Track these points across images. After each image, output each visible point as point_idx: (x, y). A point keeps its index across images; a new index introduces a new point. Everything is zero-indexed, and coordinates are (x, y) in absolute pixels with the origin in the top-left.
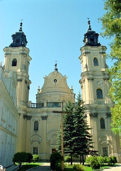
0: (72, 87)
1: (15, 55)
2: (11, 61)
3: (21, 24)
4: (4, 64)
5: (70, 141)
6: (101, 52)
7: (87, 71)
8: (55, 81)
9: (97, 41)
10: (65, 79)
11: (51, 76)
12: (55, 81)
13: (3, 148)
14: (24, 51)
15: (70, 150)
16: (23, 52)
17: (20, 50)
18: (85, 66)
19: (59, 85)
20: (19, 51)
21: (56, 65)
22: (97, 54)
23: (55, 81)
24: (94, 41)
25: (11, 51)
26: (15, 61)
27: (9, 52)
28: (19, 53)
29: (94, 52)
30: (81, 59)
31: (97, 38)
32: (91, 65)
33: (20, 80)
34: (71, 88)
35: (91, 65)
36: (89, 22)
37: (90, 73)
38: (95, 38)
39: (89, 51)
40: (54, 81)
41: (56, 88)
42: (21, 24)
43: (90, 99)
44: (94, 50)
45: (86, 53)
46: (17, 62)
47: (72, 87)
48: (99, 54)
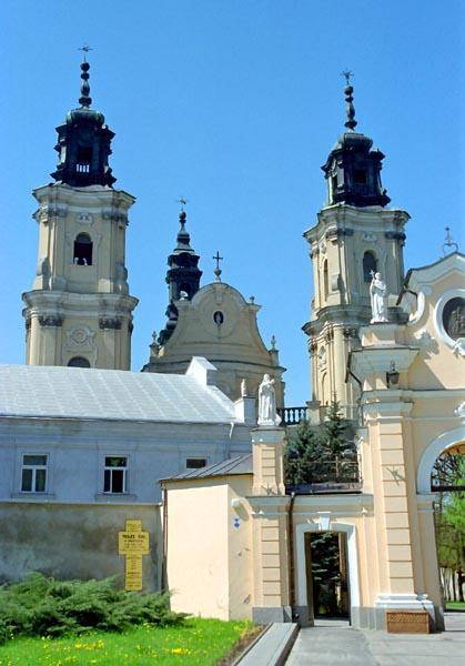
0: (273, 343)
1: (84, 221)
2: (69, 244)
3: (85, 67)
4: (46, 256)
5: (319, 544)
6: (390, 233)
7: (343, 304)
8: (218, 318)
9: (376, 183)
10: (251, 311)
11: (201, 302)
12: (218, 318)
13: (293, 602)
14: (117, 206)
15: (318, 568)
16: (115, 210)
17: (102, 200)
18: (335, 281)
19: (231, 334)
20: (98, 206)
21: (183, 218)
22: (375, 238)
23: (219, 317)
24: (365, 182)
25: (67, 203)
26: (85, 241)
27: (63, 206)
28: (97, 211)
29: (364, 229)
30: (311, 241)
31: (378, 167)
32: (357, 280)
33: (113, 323)
34: (269, 347)
35: (357, 280)
36: (350, 91)
37: (354, 311)
38: (371, 170)
39: (349, 226)
40: (215, 318)
41: (222, 346)
42: (85, 67)
43: (349, 402)
44: (368, 220)
45: (339, 232)
46: (91, 245)
47: (273, 343)
48: (383, 240)
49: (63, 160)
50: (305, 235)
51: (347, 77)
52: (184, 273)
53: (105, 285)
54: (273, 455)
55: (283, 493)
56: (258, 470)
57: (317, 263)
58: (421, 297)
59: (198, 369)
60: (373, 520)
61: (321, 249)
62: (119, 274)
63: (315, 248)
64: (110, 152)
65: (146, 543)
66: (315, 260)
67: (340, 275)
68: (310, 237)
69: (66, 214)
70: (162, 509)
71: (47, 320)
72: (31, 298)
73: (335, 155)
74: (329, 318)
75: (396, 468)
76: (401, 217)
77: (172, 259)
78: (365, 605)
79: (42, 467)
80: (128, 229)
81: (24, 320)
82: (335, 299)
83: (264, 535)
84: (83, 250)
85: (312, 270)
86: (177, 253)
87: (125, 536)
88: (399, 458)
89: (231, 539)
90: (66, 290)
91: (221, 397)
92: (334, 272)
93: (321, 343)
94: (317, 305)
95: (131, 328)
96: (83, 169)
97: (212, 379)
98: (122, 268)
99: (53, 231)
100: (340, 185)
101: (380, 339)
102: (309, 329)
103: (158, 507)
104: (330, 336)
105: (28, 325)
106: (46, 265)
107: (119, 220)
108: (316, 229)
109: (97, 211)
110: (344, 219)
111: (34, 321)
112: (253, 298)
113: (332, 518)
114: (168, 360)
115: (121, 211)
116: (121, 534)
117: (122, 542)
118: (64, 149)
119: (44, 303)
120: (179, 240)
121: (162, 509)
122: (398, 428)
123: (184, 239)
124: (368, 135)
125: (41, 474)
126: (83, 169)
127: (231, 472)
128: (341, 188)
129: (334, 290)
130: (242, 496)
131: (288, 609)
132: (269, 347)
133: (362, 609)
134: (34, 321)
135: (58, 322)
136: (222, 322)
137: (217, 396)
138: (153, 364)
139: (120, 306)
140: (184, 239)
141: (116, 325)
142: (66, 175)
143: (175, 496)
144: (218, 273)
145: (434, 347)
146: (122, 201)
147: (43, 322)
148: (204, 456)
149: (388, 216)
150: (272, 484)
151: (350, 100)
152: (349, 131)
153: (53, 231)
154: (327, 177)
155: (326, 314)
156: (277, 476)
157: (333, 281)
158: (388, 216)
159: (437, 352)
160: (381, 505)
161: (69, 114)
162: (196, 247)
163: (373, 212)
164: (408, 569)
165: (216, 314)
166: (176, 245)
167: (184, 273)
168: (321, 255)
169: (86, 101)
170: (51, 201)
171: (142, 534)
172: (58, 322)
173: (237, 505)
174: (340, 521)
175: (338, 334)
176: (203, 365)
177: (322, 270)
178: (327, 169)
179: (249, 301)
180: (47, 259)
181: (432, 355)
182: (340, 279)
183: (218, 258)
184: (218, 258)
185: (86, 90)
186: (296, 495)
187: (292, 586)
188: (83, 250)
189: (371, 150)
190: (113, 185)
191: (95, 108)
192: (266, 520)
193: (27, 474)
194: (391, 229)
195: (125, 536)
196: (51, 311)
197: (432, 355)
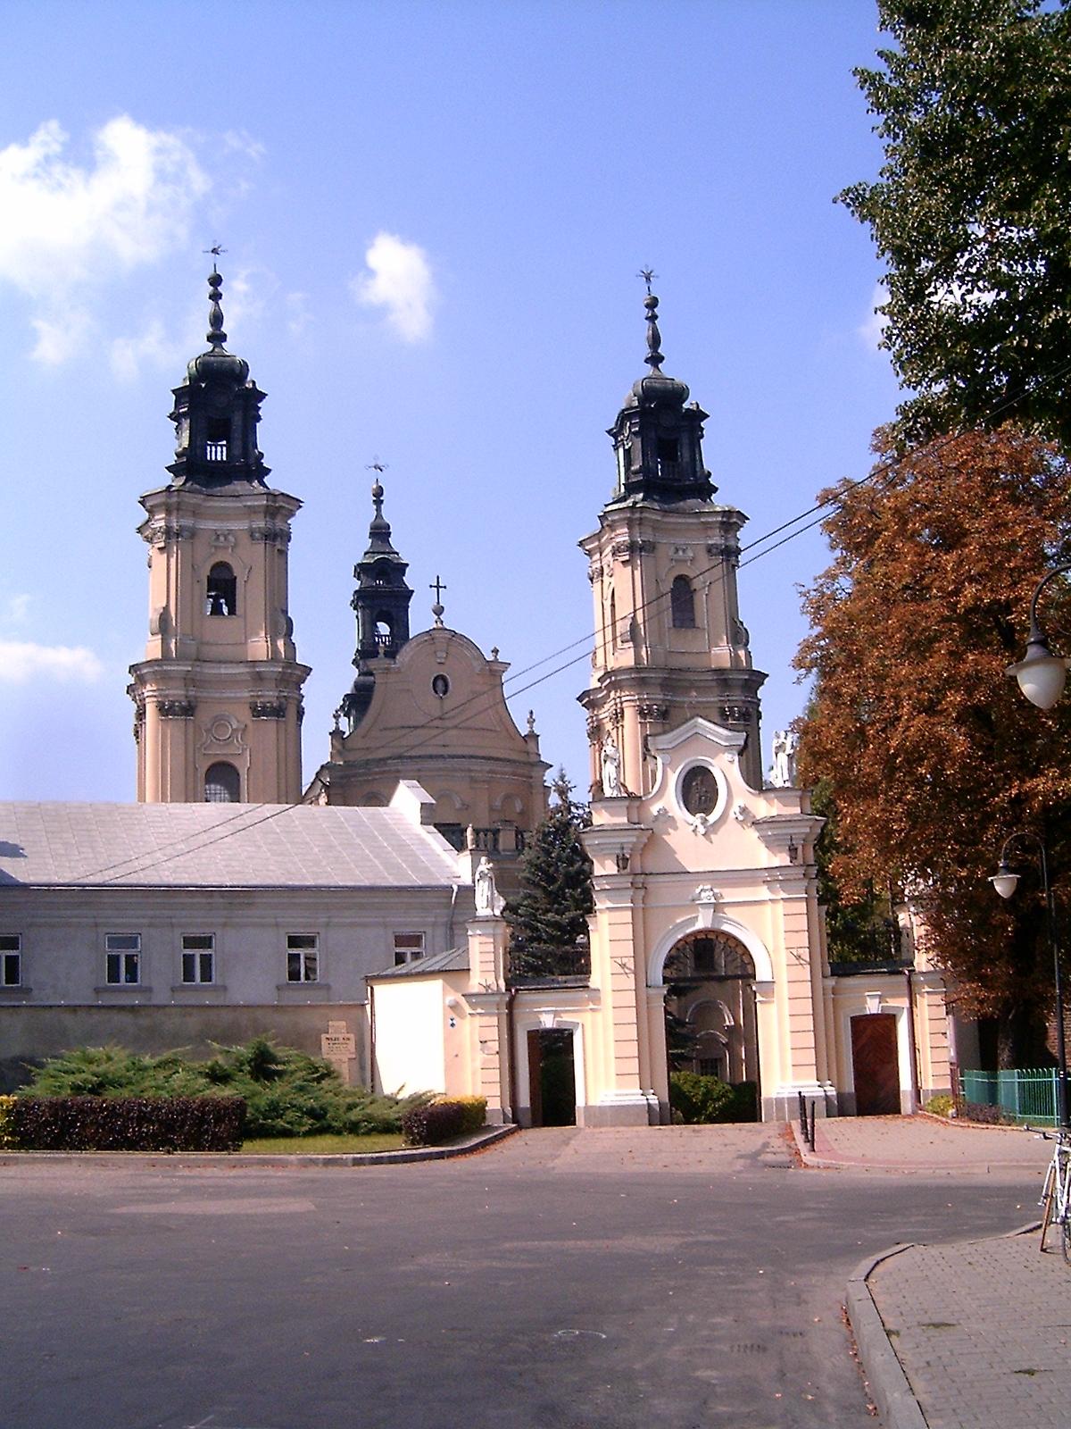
0: (531, 721)
3: (216, 281)
7: (637, 668)
8: (440, 683)
9: (694, 460)
10: (493, 671)
12: (440, 683)
30: (590, 553)
31: (696, 434)
34: (524, 731)
38: (685, 440)
45: (632, 548)
47: (531, 721)
49: (186, 444)
50: (581, 544)
51: (648, 279)
52: (382, 589)
53: (259, 647)
54: (491, 947)
55: (504, 990)
56: (475, 966)
58: (659, 761)
59: (408, 799)
60: (599, 1016)
62: (281, 625)
64: (258, 419)
65: (352, 1045)
66: (597, 585)
67: (634, 618)
69: (193, 534)
70: (368, 1007)
73: (624, 417)
74: (615, 686)
75: (625, 960)
76: (732, 520)
77: (361, 570)
78: (590, 1104)
80: (293, 548)
81: (133, 707)
82: (626, 658)
83: (481, 1030)
84: (222, 586)
85: (591, 602)
88: (628, 949)
89: (447, 1040)
90: (198, 660)
91: (442, 845)
92: (624, 609)
94: (600, 661)
95: (300, 713)
96: (217, 453)
97: (429, 815)
98: (283, 621)
99: (173, 561)
101: (612, 815)
102: (589, 700)
103: (364, 1005)
104: (618, 716)
105: (141, 715)
106: (164, 617)
107: (277, 539)
108: (598, 536)
109: (241, 525)
111: (151, 709)
112: (496, 651)
113: (556, 1013)
114: (356, 780)
115: (279, 524)
116: (324, 1036)
117: (324, 1043)
118: (186, 424)
119: (163, 678)
120: (372, 535)
121: (368, 1007)
122: (627, 916)
123: (380, 532)
124: (680, 379)
125: (206, 960)
126: (217, 453)
128: (636, 473)
130: (456, 991)
131: (509, 1110)
132: (524, 731)
133: (587, 1108)
134: (151, 709)
135: (188, 710)
136: (445, 692)
137: (436, 842)
140: (380, 532)
141: (278, 712)
142: (190, 466)
143: (382, 991)
144: (439, 611)
145: (671, 821)
146: (283, 507)
147: (163, 710)
148: (414, 931)
150: (491, 980)
151: (653, 318)
153: (173, 561)
155: (613, 680)
156: (496, 971)
157: (623, 627)
159: (676, 828)
160: (608, 999)
163: (683, 513)
164: (634, 1066)
165: (436, 679)
167: (382, 589)
168: (606, 578)
169: (217, 338)
170: (169, 512)
171: (348, 1036)
172: (188, 710)
173: (453, 1003)
174: (567, 1018)
175: (629, 713)
176: (418, 796)
177: (608, 604)
179: (490, 657)
180: (166, 609)
181: (670, 830)
182: (634, 625)
183: (438, 587)
184: (438, 587)
186: (517, 990)
188: (222, 586)
189: (685, 406)
192: (487, 1018)
193: (188, 960)
194: (716, 539)
196: (177, 693)
197: (670, 830)
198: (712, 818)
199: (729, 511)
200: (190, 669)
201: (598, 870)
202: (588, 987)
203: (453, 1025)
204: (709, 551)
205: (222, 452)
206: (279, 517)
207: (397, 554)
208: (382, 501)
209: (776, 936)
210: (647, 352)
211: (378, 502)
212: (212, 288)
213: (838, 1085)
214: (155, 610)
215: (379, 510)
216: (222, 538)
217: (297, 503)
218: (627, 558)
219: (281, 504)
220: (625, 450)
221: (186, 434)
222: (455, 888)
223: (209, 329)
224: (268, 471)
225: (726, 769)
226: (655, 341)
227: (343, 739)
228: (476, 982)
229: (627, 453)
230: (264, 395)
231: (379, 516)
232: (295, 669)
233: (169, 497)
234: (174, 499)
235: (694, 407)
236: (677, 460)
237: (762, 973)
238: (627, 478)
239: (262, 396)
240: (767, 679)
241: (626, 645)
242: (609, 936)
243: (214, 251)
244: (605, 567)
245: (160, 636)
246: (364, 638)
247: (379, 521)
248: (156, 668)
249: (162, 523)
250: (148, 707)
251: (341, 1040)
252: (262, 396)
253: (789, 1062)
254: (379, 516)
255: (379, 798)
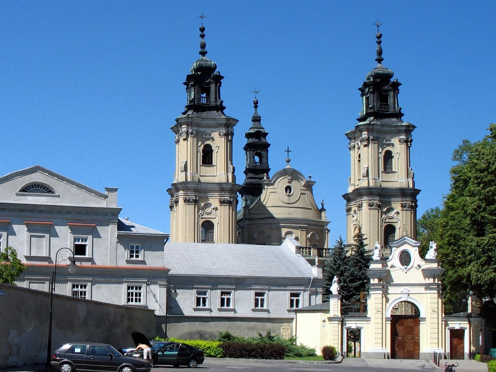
0: (322, 204)
57: (354, 154)
61: (356, 147)
63: (352, 144)
65: (289, 331)
68: (351, 136)
71: (189, 200)
72: (179, 186)
73: (366, 85)
79: (228, 297)
86: (252, 131)
87: (283, 328)
93: (354, 208)
100: (370, 106)
102: (348, 198)
104: (360, 206)
110: (372, 130)
116: (281, 328)
120: (253, 121)
123: (256, 119)
127: (322, 309)
128: (371, 108)
129: (364, 177)
137: (302, 261)
138: (246, 219)
139: (231, 190)
140: (256, 119)
149: (401, 128)
151: (379, 43)
152: (379, 65)
154: (362, 95)
158: (401, 128)
160: (373, 320)
161: (195, 64)
162: (266, 126)
166: (251, 124)
170: (188, 125)
173: (324, 320)
178: (362, 90)
180: (186, 162)
185: (203, 46)
187: (303, 367)
190: (224, 111)
191: (210, 59)
195: (283, 328)
198: (409, 267)
199: (409, 125)
200: (196, 186)
201: (372, 281)
202: (366, 317)
203: (324, 326)
204: (400, 141)
205: (204, 100)
206: (230, 127)
207: (264, 128)
208: (257, 106)
209: (429, 304)
210: (376, 57)
211: (256, 107)
212: (201, 32)
213: (47, 280)
214: (182, 162)
215: (256, 110)
216: (208, 135)
217: (237, 121)
218: (366, 143)
219: (231, 122)
220: (366, 98)
221: (193, 93)
222: (312, 278)
223: (200, 50)
224: (225, 108)
225: (414, 253)
226: (380, 53)
227: (249, 210)
228: (331, 314)
229: (367, 99)
230: (223, 77)
231: (256, 112)
232: (236, 186)
233: (188, 119)
234: (190, 120)
235: (396, 81)
236: (388, 103)
237: (422, 315)
238: (366, 110)
239: (223, 77)
240: (421, 192)
241: (365, 178)
242: (374, 300)
243: (202, 17)
244: (356, 145)
245: (184, 173)
246: (249, 163)
247: (256, 114)
248: (184, 185)
249: (185, 129)
250: (180, 199)
251: (286, 329)
252: (223, 77)
253: (429, 342)
254: (256, 112)
255: (279, 241)
